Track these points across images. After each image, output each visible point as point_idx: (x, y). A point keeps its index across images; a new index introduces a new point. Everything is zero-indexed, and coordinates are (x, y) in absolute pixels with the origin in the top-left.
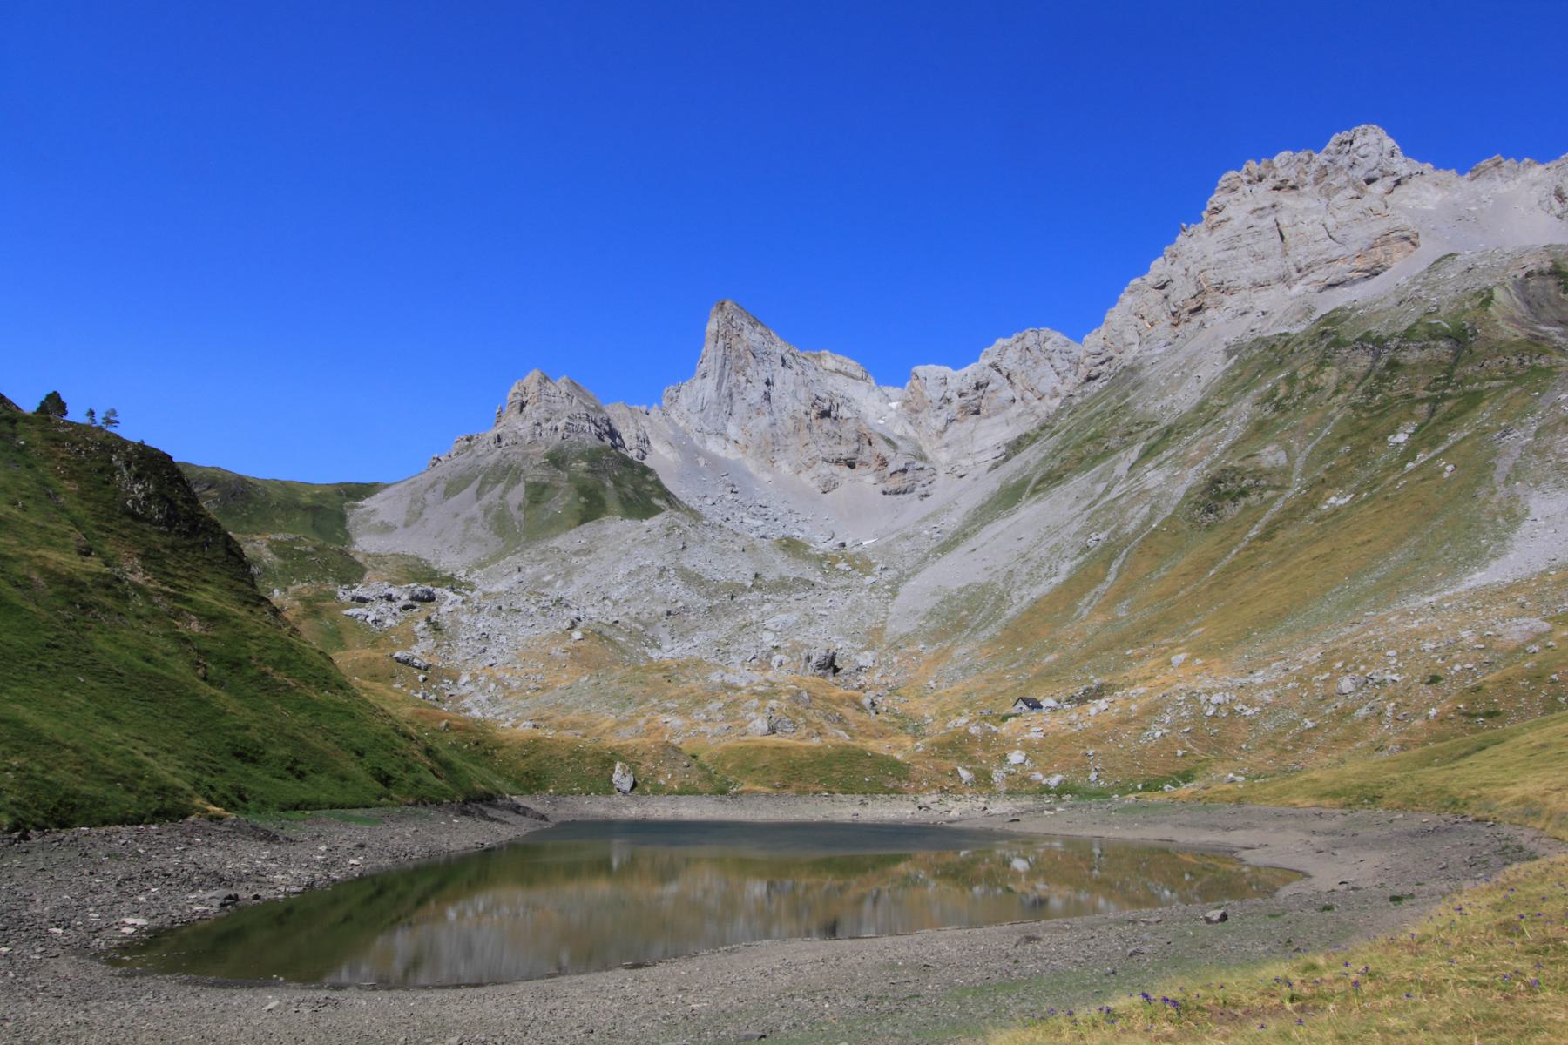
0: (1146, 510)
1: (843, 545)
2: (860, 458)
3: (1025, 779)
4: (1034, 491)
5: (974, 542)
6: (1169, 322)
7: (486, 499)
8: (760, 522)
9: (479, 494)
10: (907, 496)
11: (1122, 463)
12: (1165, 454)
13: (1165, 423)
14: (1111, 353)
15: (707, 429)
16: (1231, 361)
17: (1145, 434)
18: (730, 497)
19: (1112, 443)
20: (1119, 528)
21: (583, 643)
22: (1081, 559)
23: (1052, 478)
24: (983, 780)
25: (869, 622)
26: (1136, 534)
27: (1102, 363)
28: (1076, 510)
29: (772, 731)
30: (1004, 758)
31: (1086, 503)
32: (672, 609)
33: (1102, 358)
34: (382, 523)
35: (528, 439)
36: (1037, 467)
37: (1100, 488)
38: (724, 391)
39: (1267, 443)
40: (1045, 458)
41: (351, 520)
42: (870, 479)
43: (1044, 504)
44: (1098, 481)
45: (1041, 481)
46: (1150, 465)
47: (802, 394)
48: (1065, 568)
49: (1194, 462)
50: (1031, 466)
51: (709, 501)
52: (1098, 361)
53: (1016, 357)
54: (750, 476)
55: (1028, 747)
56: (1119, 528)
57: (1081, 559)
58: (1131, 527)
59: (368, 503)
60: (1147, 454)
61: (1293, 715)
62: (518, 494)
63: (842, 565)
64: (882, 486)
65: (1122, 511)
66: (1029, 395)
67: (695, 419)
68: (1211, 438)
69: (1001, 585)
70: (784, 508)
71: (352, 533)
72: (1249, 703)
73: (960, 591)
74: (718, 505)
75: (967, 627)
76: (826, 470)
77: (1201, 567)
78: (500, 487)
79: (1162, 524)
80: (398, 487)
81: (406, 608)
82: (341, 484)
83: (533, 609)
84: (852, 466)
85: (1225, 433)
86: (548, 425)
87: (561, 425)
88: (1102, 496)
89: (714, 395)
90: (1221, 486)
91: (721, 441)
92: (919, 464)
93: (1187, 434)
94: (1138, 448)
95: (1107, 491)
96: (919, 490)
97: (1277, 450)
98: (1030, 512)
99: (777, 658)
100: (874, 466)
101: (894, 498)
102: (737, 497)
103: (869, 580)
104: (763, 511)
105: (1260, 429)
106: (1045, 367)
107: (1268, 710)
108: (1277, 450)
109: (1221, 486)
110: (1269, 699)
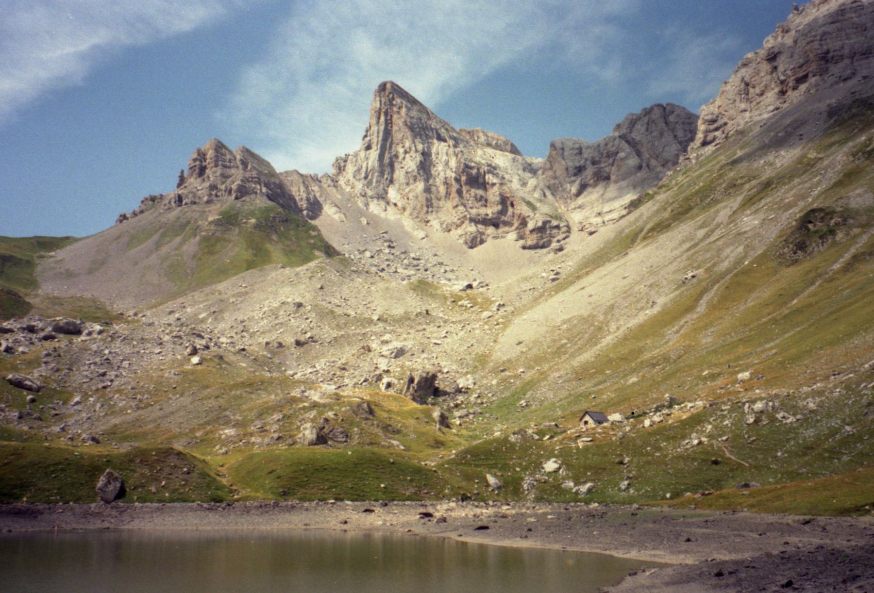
0: (741, 249)
1: (470, 286)
2: (503, 218)
3: (558, 487)
4: (645, 238)
5: (584, 282)
6: (777, 90)
7: (165, 250)
8: (412, 272)
9: (158, 245)
10: (545, 251)
11: (723, 212)
12: (763, 202)
13: (764, 177)
14: (725, 120)
15: (370, 193)
16: (832, 121)
17: (747, 186)
18: (387, 251)
19: (717, 195)
20: (714, 265)
21: (200, 367)
22: (677, 293)
23: (661, 227)
24: (511, 489)
25: (479, 350)
26: (728, 271)
27: (717, 129)
28: (677, 252)
29: (321, 439)
30: (539, 466)
31: (688, 245)
32: (302, 338)
33: (716, 125)
34: (67, 271)
35: (206, 199)
36: (650, 218)
37: (701, 233)
38: (386, 160)
39: (856, 188)
40: (658, 211)
41: (39, 269)
42: (512, 236)
43: (653, 246)
44: (701, 227)
45: (652, 230)
46: (748, 212)
47: (453, 163)
48: (662, 300)
49: (789, 206)
50: (645, 217)
51: (368, 254)
52: (712, 127)
53: (643, 129)
54: (407, 233)
55: (565, 456)
56: (714, 265)
57: (677, 293)
58: (726, 264)
59: (60, 254)
60: (749, 202)
61: (835, 423)
62: (192, 246)
63: (465, 302)
64: (521, 242)
65: (720, 250)
66: (653, 162)
67: (359, 186)
68: (807, 185)
69: (601, 318)
70: (434, 260)
71: (39, 279)
72: (793, 409)
73: (564, 322)
74: (376, 257)
75: (565, 353)
76: (472, 228)
77: (783, 298)
78: (178, 239)
79: (752, 263)
80: (87, 241)
81: (46, 338)
82: (36, 237)
83: (167, 338)
84: (496, 226)
85: (820, 182)
86: (223, 187)
87: (234, 187)
88: (702, 240)
89: (376, 164)
90: (810, 226)
91: (383, 203)
92: (554, 223)
93: (784, 184)
94: (739, 199)
95: (707, 235)
96: (554, 245)
97: (866, 192)
98: (640, 256)
99: (385, 380)
100: (516, 224)
101: (532, 252)
102: (393, 251)
103: (486, 314)
104: (415, 262)
105: (849, 177)
106: (668, 137)
107: (809, 419)
108: (866, 192)
109: (810, 226)
110: (812, 406)
